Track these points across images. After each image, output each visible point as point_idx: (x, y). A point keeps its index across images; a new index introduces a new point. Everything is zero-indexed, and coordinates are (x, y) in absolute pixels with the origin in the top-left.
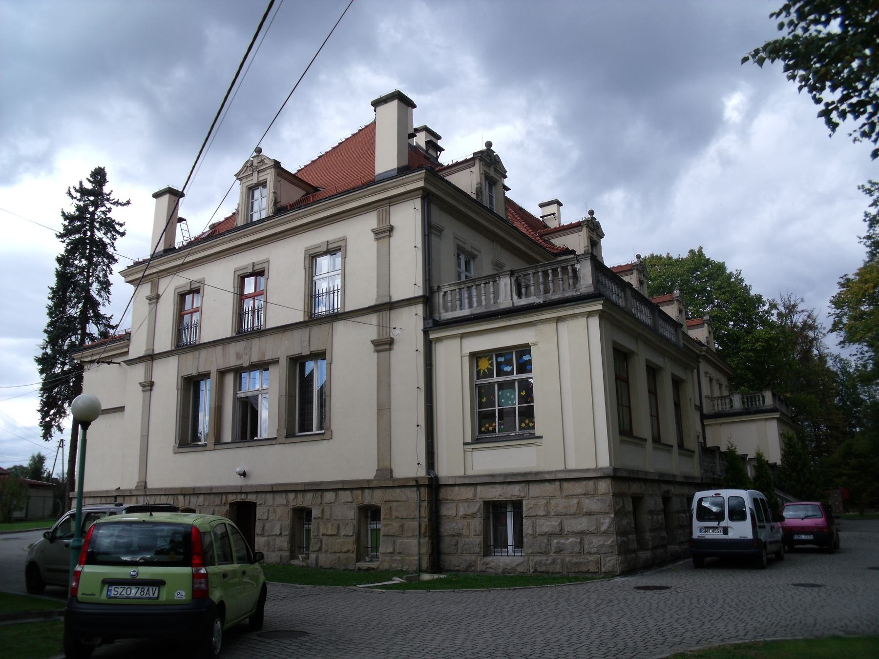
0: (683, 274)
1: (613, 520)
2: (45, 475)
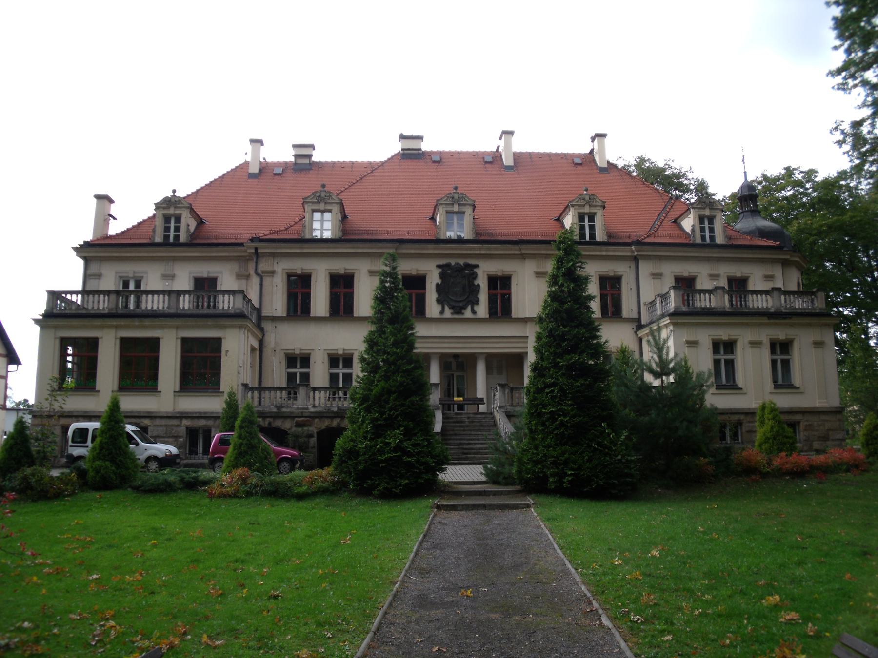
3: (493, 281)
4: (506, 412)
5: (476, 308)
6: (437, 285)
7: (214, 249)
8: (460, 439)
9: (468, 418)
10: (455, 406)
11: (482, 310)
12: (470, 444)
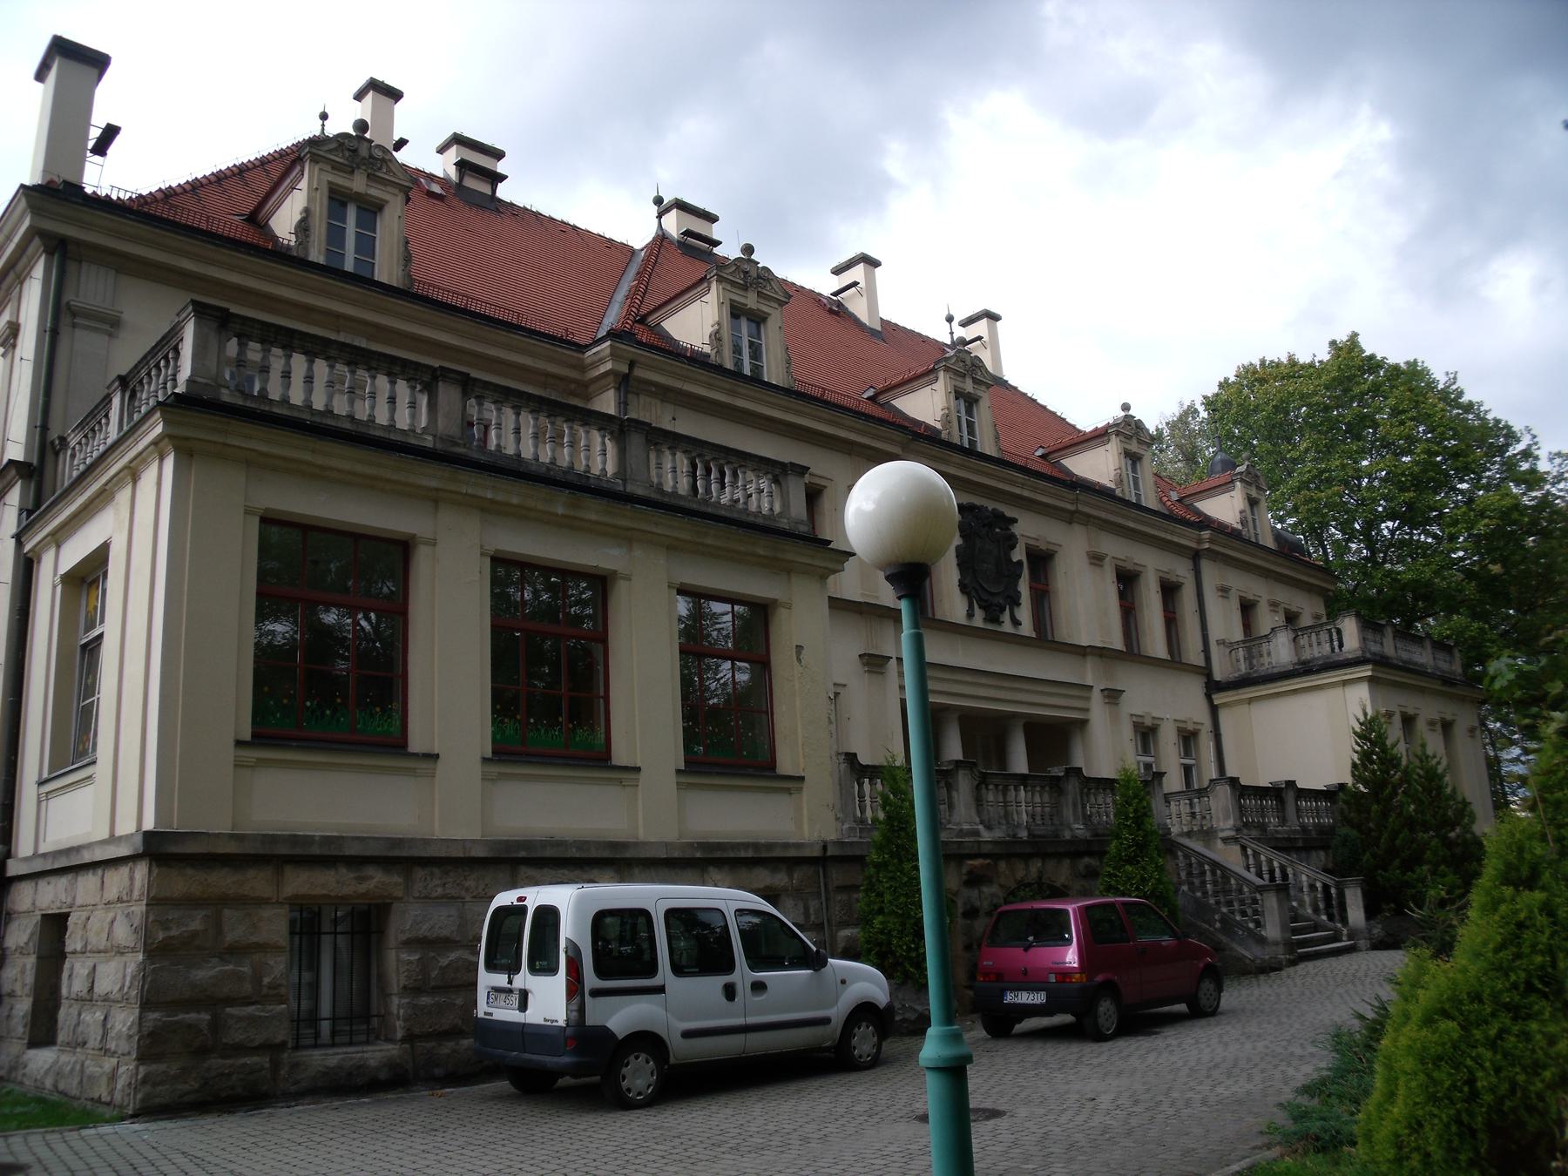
0: (1315, 393)
1: (142, 967)
2: (1448, 790)
7: (502, 336)
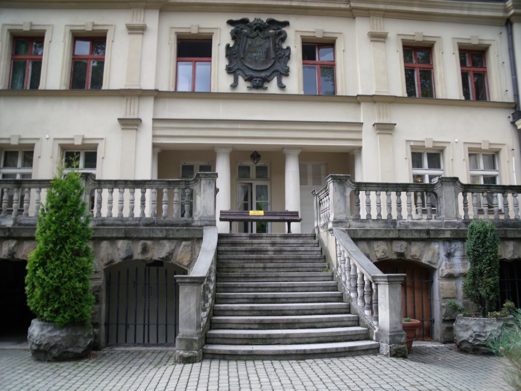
3: (310, 48)
4: (349, 232)
5: (285, 81)
6: (228, 46)
8: (257, 288)
9: (273, 244)
10: (255, 224)
11: (294, 83)
12: (275, 300)
